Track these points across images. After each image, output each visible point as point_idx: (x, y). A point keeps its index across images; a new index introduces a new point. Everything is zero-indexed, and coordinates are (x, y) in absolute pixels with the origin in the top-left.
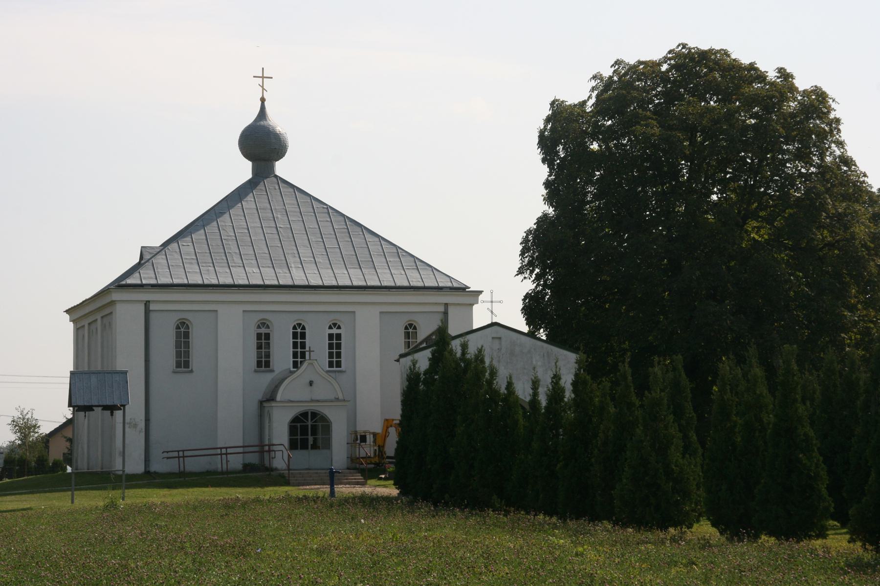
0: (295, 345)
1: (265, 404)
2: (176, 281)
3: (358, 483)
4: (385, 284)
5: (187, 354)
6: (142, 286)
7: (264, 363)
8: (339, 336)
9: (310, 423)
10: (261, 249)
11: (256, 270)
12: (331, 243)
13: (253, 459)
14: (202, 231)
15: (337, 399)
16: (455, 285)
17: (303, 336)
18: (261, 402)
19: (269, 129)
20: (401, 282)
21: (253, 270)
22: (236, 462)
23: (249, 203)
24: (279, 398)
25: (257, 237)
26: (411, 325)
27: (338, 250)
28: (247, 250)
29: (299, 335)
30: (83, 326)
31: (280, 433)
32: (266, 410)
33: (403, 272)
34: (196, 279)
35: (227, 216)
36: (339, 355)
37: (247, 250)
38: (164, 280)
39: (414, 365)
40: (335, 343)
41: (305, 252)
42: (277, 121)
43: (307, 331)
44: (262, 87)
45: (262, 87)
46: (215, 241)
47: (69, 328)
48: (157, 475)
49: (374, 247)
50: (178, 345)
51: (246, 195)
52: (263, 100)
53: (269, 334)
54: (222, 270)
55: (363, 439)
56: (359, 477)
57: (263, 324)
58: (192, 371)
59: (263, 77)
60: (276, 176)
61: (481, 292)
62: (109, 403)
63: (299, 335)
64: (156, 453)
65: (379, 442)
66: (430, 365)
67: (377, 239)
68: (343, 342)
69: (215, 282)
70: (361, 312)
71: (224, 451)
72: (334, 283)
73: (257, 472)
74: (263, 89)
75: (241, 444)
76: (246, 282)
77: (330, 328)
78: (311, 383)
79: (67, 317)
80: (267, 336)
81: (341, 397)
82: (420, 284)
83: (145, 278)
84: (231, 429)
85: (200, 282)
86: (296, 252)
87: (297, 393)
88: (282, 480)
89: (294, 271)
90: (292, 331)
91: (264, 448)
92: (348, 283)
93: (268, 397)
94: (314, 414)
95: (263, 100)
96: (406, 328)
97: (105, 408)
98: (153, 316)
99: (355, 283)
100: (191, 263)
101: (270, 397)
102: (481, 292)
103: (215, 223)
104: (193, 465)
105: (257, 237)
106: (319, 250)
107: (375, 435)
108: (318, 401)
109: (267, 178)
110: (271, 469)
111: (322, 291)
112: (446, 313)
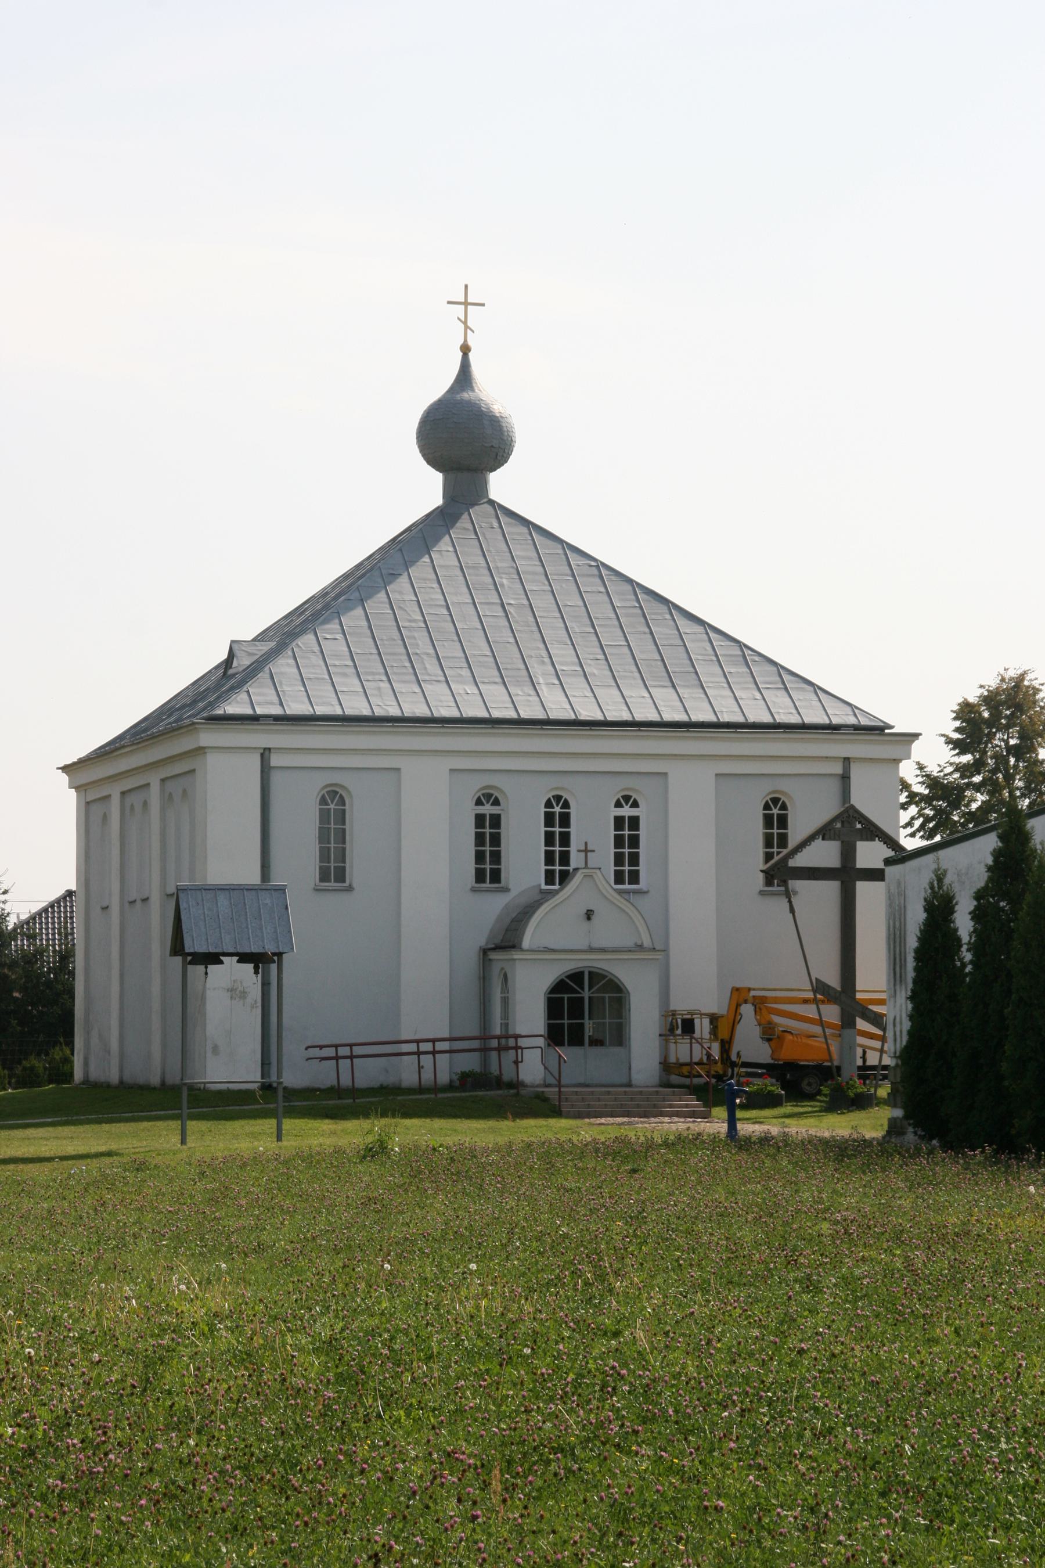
0: (549, 839)
1: (493, 956)
2: (321, 710)
3: (694, 1115)
4: (725, 718)
5: (496, 857)
6: (255, 719)
7: (488, 868)
8: (634, 822)
9: (586, 994)
10: (477, 648)
11: (471, 689)
12: (610, 636)
13: (470, 1063)
14: (359, 611)
15: (640, 948)
16: (864, 721)
17: (565, 819)
18: (485, 952)
19: (480, 407)
20: (757, 714)
21: (464, 689)
22: (444, 1069)
23: (443, 553)
24: (526, 943)
25: (467, 623)
26: (776, 801)
27: (626, 650)
28: (449, 650)
29: (558, 818)
30: (108, 797)
31: (530, 1016)
32: (496, 969)
33: (758, 696)
34: (356, 706)
35: (403, 580)
36: (634, 859)
37: (449, 650)
38: (297, 707)
39: (940, 880)
40: (627, 835)
41: (562, 653)
42: (493, 391)
43: (573, 811)
44: (465, 323)
45: (465, 323)
46: (386, 633)
47: (65, 802)
48: (291, 1093)
49: (697, 646)
50: (324, 836)
51: (437, 540)
52: (465, 349)
53: (499, 816)
54: (407, 689)
55: (688, 1026)
56: (693, 1102)
57: (488, 797)
58: (350, 889)
59: (466, 304)
60: (492, 503)
61: (916, 736)
62: (255, 949)
63: (558, 818)
64: (293, 1051)
65: (724, 1034)
66: (990, 879)
67: (701, 629)
68: (643, 833)
69: (394, 711)
70: (676, 772)
71: (344, 1051)
72: (626, 716)
73: (482, 1088)
74: (467, 327)
75: (447, 1035)
76: (454, 713)
77: (618, 805)
78: (589, 915)
79: (64, 778)
80: (496, 821)
81: (647, 943)
82: (794, 719)
83: (259, 704)
84: (427, 1004)
85: (366, 712)
86: (544, 653)
87: (559, 936)
88: (542, 1105)
89: (544, 691)
90: (543, 810)
91: (495, 1041)
92: (653, 717)
93: (498, 941)
94: (596, 976)
95: (465, 349)
96: (767, 807)
97: (244, 958)
98: (276, 778)
99: (667, 717)
100: (345, 675)
101: (506, 940)
102: (916, 736)
103: (382, 595)
104: (369, 1073)
105: (467, 623)
106: (589, 650)
107: (714, 1019)
108: (603, 950)
109: (473, 505)
110: (515, 1085)
111: (772, 734)
112: (845, 778)
